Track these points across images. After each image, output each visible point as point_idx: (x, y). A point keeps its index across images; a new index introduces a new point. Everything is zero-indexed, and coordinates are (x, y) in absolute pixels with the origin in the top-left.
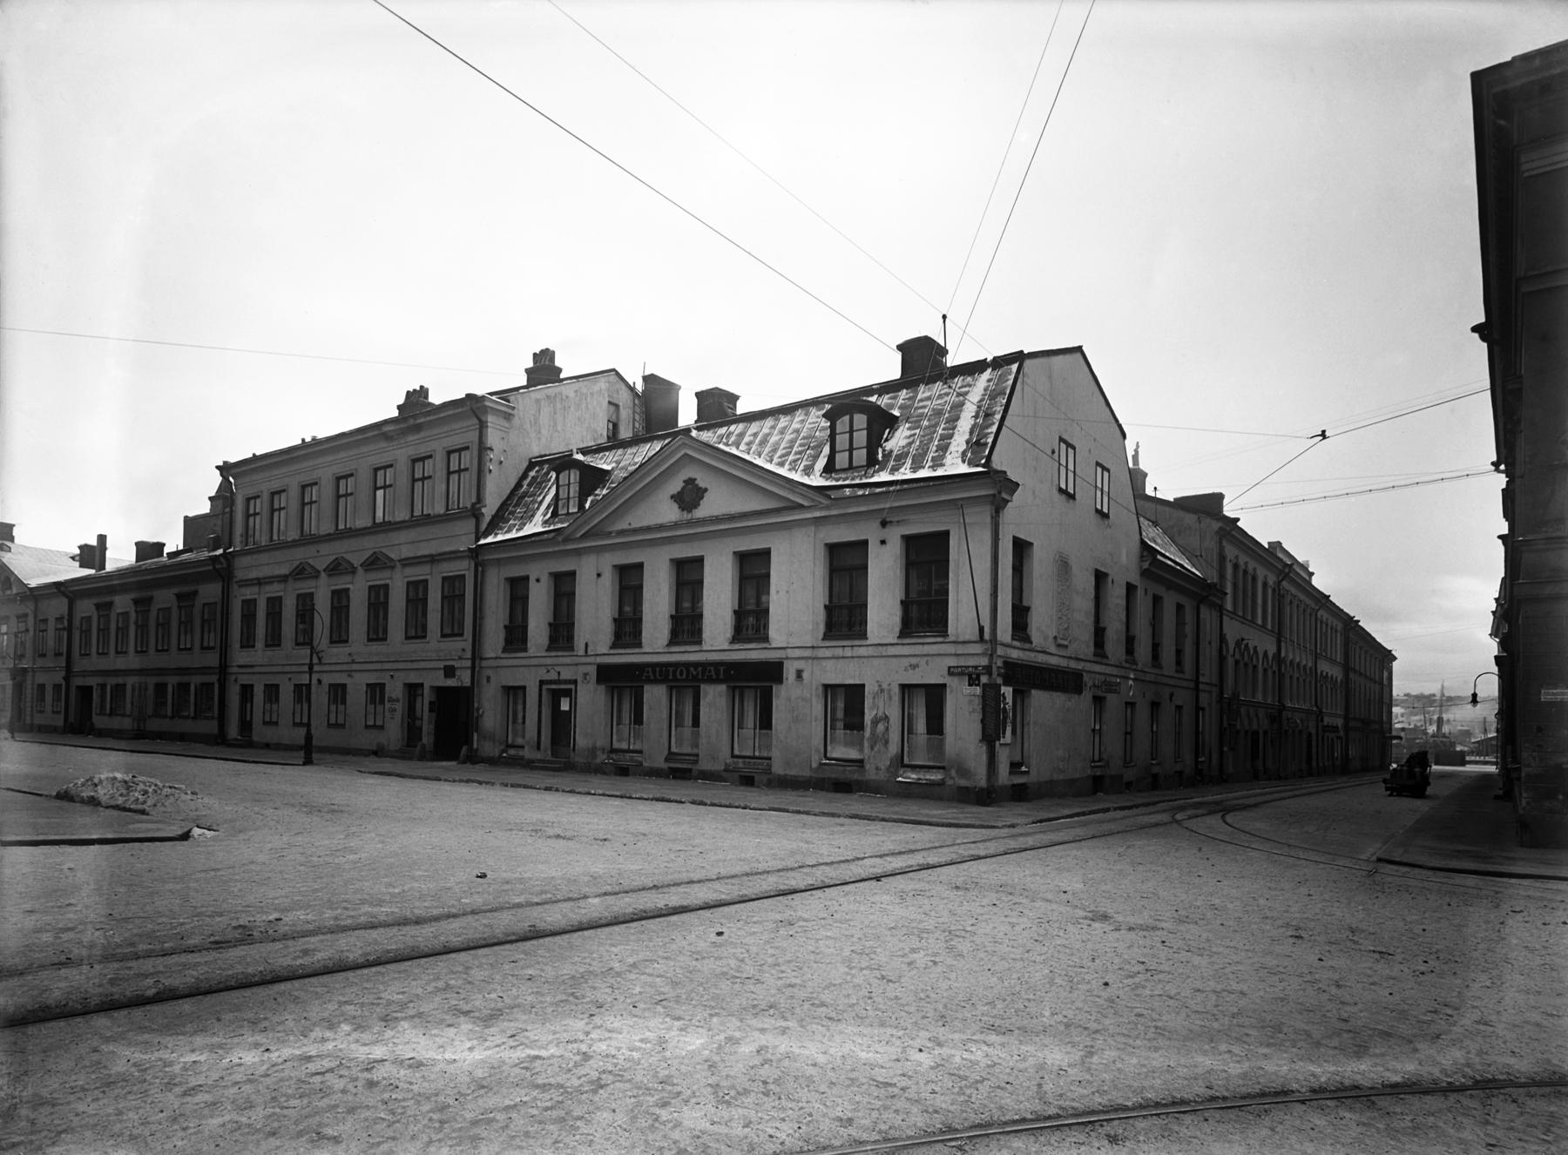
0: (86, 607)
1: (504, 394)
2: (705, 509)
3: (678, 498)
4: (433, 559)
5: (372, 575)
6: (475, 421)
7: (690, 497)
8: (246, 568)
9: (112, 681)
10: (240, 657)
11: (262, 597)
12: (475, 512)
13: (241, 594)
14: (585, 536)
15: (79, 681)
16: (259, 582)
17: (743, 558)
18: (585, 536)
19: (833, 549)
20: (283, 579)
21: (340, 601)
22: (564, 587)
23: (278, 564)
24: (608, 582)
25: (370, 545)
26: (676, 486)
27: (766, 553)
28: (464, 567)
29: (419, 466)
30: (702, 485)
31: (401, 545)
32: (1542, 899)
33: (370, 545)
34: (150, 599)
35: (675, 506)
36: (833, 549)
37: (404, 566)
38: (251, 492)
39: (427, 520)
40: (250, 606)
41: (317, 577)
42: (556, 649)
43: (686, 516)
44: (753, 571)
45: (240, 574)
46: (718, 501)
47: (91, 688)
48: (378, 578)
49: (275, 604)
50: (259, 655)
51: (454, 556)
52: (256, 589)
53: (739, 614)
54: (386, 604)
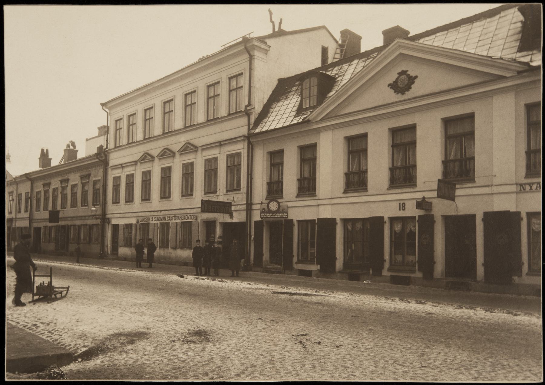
0: (39, 187)
1: (262, 39)
2: (417, 89)
3: (394, 86)
4: (220, 144)
5: (163, 161)
6: (247, 56)
7: (404, 83)
8: (115, 159)
9: (402, 202)
10: (111, 208)
11: (123, 174)
12: (247, 113)
13: (112, 174)
14: (322, 120)
15: (35, 225)
16: (122, 166)
17: (303, 149)
18: (322, 120)
19: (349, 140)
20: (135, 163)
21: (166, 174)
22: (308, 156)
23: (135, 153)
24: (341, 149)
25: (183, 139)
26: (392, 77)
27: (365, 136)
28: (241, 148)
29: (212, 90)
30: (412, 73)
31: (201, 137)
32: (104, 300)
33: (183, 139)
34: (68, 180)
35: (392, 91)
36: (349, 140)
37: (203, 150)
38: (117, 117)
39: (134, 142)
40: (117, 179)
41: (196, 151)
42: (528, 178)
43: (400, 97)
44: (459, 133)
45: (112, 163)
46: (427, 82)
47: (41, 228)
48: (166, 163)
49: (130, 178)
50: (123, 207)
51: (232, 141)
52: (119, 171)
53: (300, 181)
54: (192, 173)
